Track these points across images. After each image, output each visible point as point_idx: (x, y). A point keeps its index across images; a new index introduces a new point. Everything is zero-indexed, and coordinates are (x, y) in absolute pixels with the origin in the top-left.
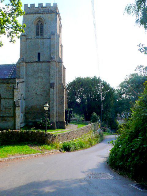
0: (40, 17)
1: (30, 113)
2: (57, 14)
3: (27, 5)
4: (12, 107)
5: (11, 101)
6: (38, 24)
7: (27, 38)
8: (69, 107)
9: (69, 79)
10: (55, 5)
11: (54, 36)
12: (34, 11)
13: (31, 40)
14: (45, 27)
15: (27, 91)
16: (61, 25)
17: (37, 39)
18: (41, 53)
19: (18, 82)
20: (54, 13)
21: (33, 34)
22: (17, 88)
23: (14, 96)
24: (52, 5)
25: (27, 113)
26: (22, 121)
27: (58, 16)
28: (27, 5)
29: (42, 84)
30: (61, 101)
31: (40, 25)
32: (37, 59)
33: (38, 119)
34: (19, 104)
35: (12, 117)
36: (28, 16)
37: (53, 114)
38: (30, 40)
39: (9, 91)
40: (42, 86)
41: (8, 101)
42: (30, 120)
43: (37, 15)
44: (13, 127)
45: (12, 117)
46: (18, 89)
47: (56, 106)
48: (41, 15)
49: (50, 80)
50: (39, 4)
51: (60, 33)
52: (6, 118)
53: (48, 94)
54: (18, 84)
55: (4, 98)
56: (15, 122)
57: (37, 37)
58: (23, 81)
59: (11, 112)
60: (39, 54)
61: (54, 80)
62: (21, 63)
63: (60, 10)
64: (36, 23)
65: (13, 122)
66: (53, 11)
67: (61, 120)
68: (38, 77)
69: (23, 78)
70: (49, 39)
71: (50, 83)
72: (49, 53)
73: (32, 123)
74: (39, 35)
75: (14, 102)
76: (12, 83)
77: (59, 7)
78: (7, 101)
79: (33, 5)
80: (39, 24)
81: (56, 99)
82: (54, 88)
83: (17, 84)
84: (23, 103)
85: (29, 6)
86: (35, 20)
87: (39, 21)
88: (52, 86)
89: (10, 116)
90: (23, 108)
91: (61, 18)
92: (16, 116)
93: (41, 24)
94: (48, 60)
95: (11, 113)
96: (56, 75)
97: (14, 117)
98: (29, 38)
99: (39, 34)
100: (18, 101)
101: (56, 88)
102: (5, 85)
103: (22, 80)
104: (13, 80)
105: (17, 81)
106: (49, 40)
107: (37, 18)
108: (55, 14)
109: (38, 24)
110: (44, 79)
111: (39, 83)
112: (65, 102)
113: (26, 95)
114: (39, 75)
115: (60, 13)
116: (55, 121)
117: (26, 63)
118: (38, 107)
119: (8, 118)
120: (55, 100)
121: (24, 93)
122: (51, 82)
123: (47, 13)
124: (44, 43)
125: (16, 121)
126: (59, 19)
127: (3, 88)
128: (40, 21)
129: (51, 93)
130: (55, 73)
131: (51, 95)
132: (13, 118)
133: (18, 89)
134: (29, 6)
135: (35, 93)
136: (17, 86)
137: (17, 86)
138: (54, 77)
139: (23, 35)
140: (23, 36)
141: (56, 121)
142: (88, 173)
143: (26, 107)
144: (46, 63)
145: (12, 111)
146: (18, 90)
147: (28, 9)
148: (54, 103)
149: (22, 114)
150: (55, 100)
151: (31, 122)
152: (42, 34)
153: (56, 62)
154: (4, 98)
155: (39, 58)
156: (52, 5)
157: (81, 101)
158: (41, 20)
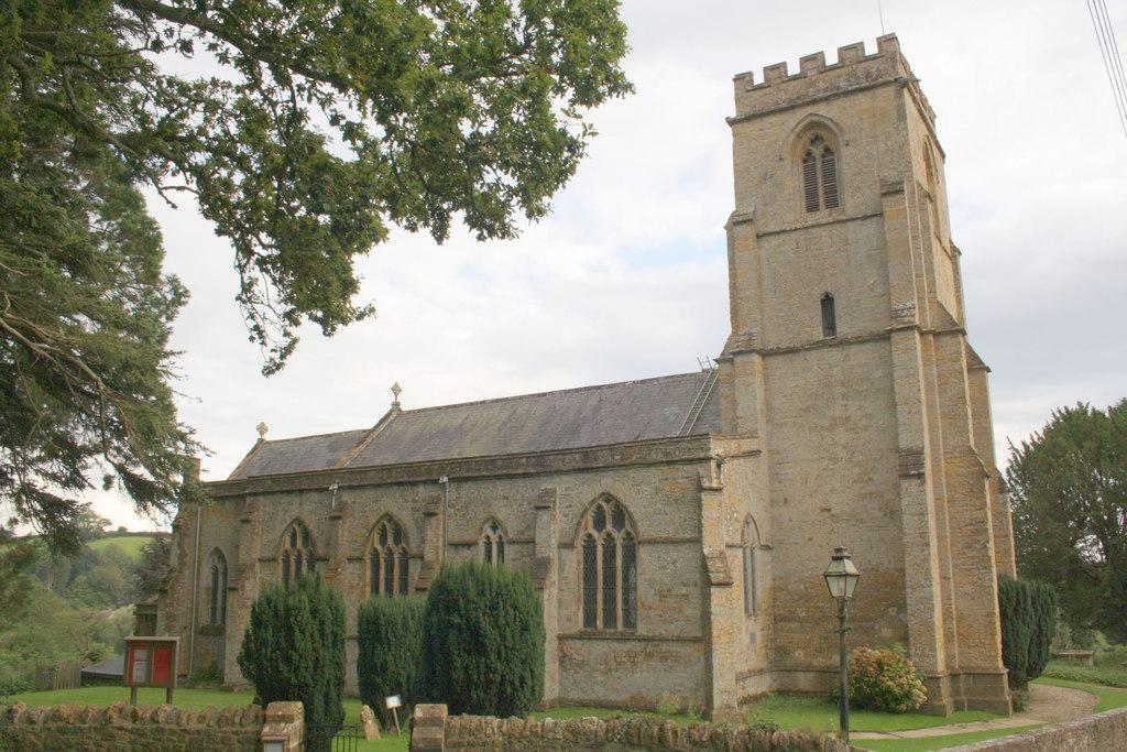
0: (815, 118)
1: (801, 621)
2: (907, 84)
3: (750, 74)
4: (695, 585)
5: (684, 558)
6: (809, 154)
7: (762, 230)
10: (888, 41)
12: (782, 98)
13: (782, 237)
15: (778, 501)
16: (937, 143)
17: (813, 226)
18: (836, 296)
19: (720, 451)
20: (885, 84)
21: (788, 205)
22: (714, 485)
23: (699, 527)
24: (871, 49)
25: (784, 614)
26: (756, 661)
27: (911, 94)
28: (750, 74)
30: (969, 547)
31: (818, 158)
32: (821, 328)
34: (727, 572)
35: (695, 640)
36: (753, 128)
37: (930, 627)
38: (775, 241)
39: (676, 501)
40: (857, 470)
42: (799, 654)
43: (801, 114)
44: (702, 693)
45: (695, 640)
46: (719, 490)
47: (944, 578)
48: (822, 110)
49: (897, 434)
50: (804, 61)
51: (930, 175)
52: (664, 647)
53: (893, 513)
54: (719, 466)
55: (653, 542)
56: (709, 668)
57: (812, 218)
58: (754, 448)
59: (688, 611)
60: (827, 302)
61: (924, 434)
62: (738, 360)
63: (918, 58)
64: (800, 152)
65: (698, 668)
66: (879, 75)
67: (978, 661)
68: (832, 427)
69: (753, 435)
70: (874, 219)
71: (897, 450)
72: (878, 291)
73: (811, 675)
74: (822, 206)
75: (704, 559)
76: (691, 461)
77: (907, 49)
78: (672, 553)
80: (817, 151)
81: (940, 538)
82: (921, 476)
83: (713, 464)
84: (758, 565)
85: (759, 79)
86: (793, 136)
87: (812, 142)
88: (910, 464)
89: (684, 635)
90: (759, 594)
91: (930, 110)
92: (715, 633)
93: (827, 150)
95: (687, 620)
96: (930, 406)
97: (704, 639)
98: (772, 227)
99: (821, 199)
100: (722, 556)
101: (936, 473)
102: (654, 475)
103: (748, 445)
104: (695, 444)
105: (717, 448)
106: (871, 226)
107: (801, 125)
108: (890, 91)
109: (809, 154)
110: (866, 428)
111: (842, 454)
112: (992, 553)
113: (774, 521)
114: (838, 411)
115: (917, 75)
116: (941, 667)
117: (765, 354)
119: (676, 648)
120: (934, 542)
121: (760, 514)
122: (903, 444)
123: (847, 93)
124: (847, 242)
125: (715, 662)
126: (916, 114)
127: (648, 490)
129: (904, 502)
130: (923, 395)
131: (905, 518)
132: (702, 646)
133: (719, 490)
134: (759, 79)
136: (714, 475)
137: (714, 475)
138: (920, 412)
139: (741, 219)
140: (737, 223)
141: (948, 666)
143: (777, 589)
144: (869, 346)
145: (692, 610)
147: (760, 92)
148: (926, 560)
149: (756, 626)
150: (934, 542)
151: (808, 669)
152: (833, 201)
153: (922, 334)
154: (653, 542)
155: (830, 326)
156: (871, 49)
157: (1106, 551)
158: (822, 133)
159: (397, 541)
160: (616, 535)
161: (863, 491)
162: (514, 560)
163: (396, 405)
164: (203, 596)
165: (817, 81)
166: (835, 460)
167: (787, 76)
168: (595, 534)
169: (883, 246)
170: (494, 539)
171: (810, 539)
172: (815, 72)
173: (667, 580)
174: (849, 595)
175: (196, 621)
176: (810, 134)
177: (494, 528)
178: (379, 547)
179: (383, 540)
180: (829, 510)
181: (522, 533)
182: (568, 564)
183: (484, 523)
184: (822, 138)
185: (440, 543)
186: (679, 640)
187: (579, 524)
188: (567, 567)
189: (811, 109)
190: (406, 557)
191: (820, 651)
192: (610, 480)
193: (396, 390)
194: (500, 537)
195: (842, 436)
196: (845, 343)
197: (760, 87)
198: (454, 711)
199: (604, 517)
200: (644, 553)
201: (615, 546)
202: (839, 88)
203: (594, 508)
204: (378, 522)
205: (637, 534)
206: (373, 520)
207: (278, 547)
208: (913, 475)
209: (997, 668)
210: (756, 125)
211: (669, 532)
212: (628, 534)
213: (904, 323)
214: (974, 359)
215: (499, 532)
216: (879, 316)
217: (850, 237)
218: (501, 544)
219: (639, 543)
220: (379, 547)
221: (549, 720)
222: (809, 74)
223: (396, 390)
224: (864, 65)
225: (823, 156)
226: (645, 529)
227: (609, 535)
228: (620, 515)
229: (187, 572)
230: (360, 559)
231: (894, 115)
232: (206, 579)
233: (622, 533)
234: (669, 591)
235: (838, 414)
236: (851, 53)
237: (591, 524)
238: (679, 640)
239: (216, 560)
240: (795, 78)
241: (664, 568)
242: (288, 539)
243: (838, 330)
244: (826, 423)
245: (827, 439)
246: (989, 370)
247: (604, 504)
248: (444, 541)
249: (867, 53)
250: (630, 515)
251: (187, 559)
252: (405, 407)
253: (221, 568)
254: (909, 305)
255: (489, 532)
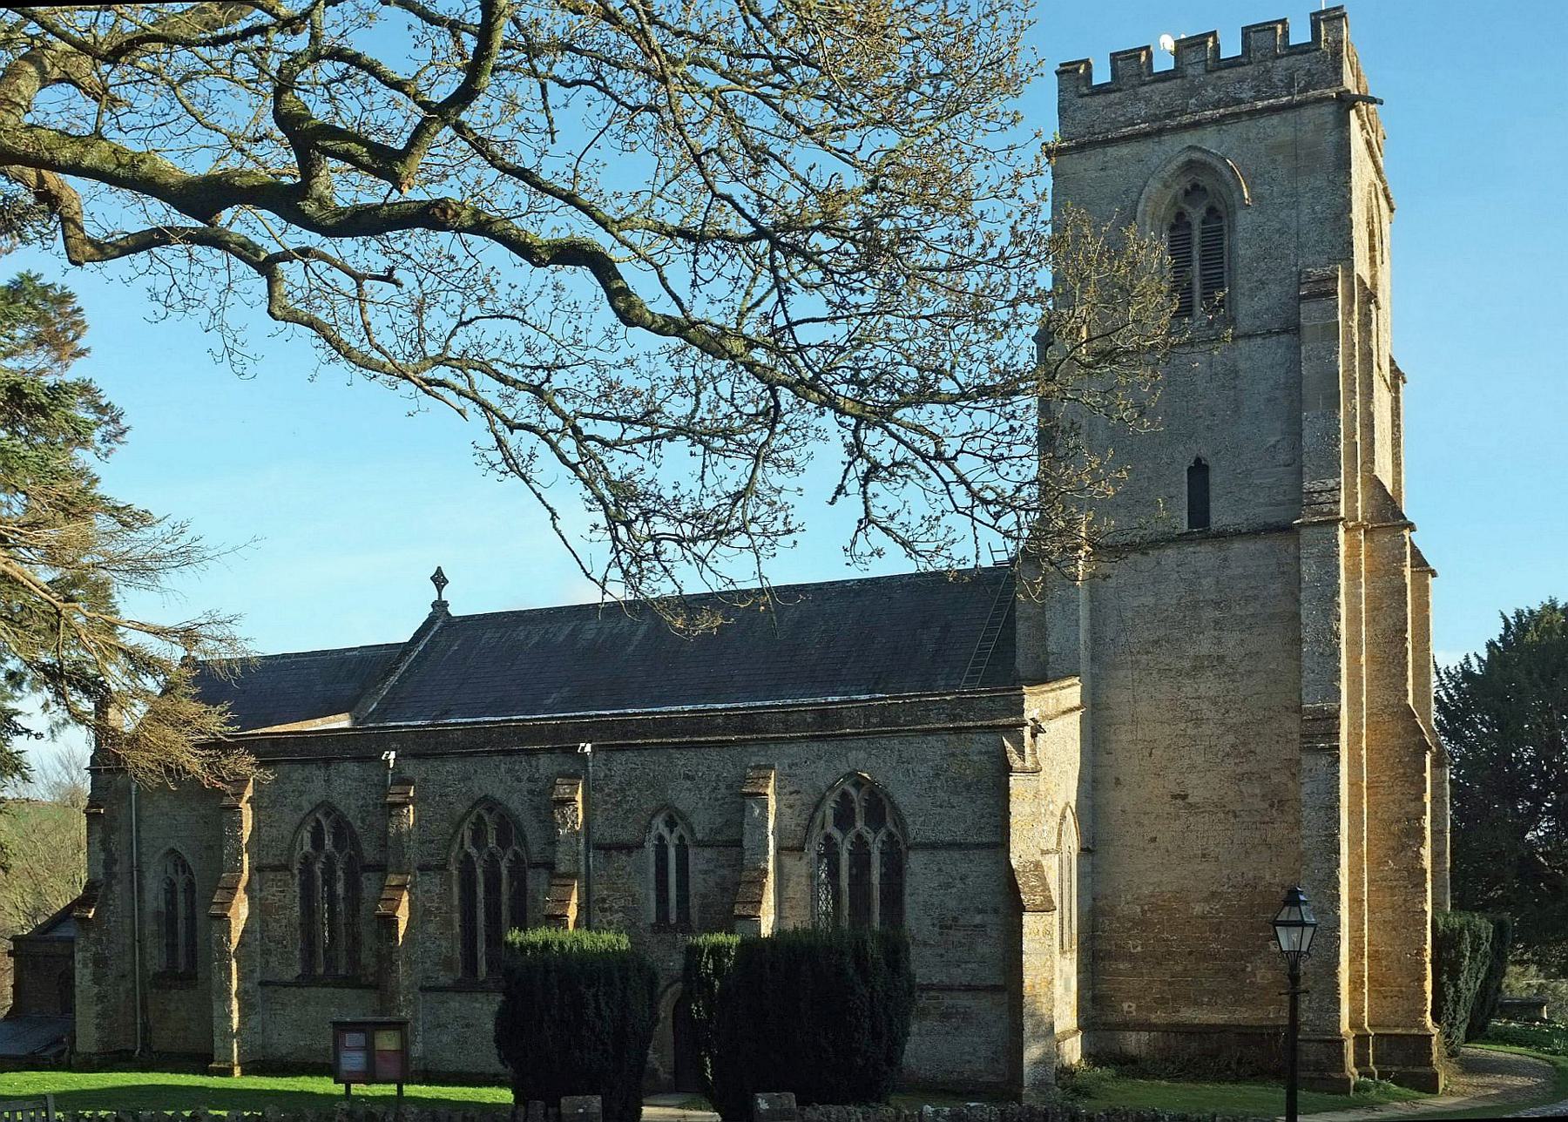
0: (1196, 155)
4: (996, 911)
5: (976, 868)
6: (1180, 215)
8: (1460, 905)
9: (1460, 636)
11: (1325, 302)
14: (1246, 234)
22: (1029, 764)
27: (1359, 116)
29: (1234, 718)
33: (1196, 1003)
35: (995, 989)
36: (1075, 163)
39: (968, 787)
40: (1231, 738)
41: (964, 868)
43: (1174, 149)
46: (1036, 771)
48: (1209, 140)
52: (947, 1000)
55: (932, 846)
59: (983, 949)
60: (1199, 471)
68: (1197, 669)
70: (1284, 338)
72: (1283, 457)
73: (1144, 1036)
79: (1131, 63)
80: (1196, 215)
93: (1211, 211)
94: (1275, 516)
109: (1180, 215)
111: (1207, 710)
114: (1205, 646)
118: (1198, 909)
119: (964, 1001)
124: (1235, 373)
126: (1363, 146)
128: (1195, 187)
135: (1175, 797)
142: (789, 106)
146: (1041, 782)
147: (1099, 100)
154: (932, 846)
155: (1199, 511)
158: (1205, 181)
159: (503, 841)
160: (870, 837)
161: (1239, 770)
162: (706, 872)
163: (440, 605)
164: (151, 927)
165: (1203, 86)
166: (1198, 722)
167: (1151, 73)
168: (837, 835)
169: (1295, 384)
170: (671, 841)
171: (1154, 840)
172: (1200, 69)
173: (952, 904)
174: (1304, 949)
175: (142, 965)
176: (1180, 186)
177: (671, 824)
178: (473, 851)
179: (478, 837)
180: (1184, 797)
181: (719, 831)
182: (794, 878)
183: (653, 816)
184: (1204, 189)
185: (582, 847)
186: (969, 988)
187: (812, 819)
188: (791, 884)
189: (1189, 138)
190: (519, 870)
191: (1162, 1002)
192: (862, 755)
193: (439, 580)
194: (681, 838)
195: (1209, 685)
196: (1222, 536)
197: (1102, 89)
198: (802, 1102)
199: (853, 810)
200: (916, 862)
201: (869, 853)
202: (1239, 102)
203: (835, 796)
204: (469, 813)
205: (905, 835)
206: (461, 809)
207: (291, 848)
208: (1323, 749)
209: (1424, 1027)
210: (1096, 158)
211: (958, 833)
212: (890, 835)
213: (1322, 514)
214: (1419, 562)
215: (678, 830)
216: (1280, 498)
217: (1242, 365)
218: (682, 850)
219: (909, 848)
220: (473, 851)
221: (928, 1109)
222: (1190, 71)
223: (439, 580)
224: (1284, 62)
225: (1204, 222)
226: (917, 829)
227: (859, 836)
228: (878, 806)
229: (117, 889)
230: (442, 868)
231: (1330, 158)
232: (154, 897)
233: (882, 835)
234: (955, 919)
235: (1204, 651)
236: (1262, 37)
237: (830, 819)
238: (969, 988)
239: (170, 869)
240: (1166, 76)
241: (948, 886)
242: (307, 836)
243: (1213, 519)
244: (1187, 664)
245: (1188, 690)
246: (1434, 574)
247: (853, 791)
248: (587, 843)
249: (1294, 41)
250: (895, 808)
251: (116, 868)
252: (455, 610)
253: (181, 881)
254: (1331, 483)
255: (659, 825)
